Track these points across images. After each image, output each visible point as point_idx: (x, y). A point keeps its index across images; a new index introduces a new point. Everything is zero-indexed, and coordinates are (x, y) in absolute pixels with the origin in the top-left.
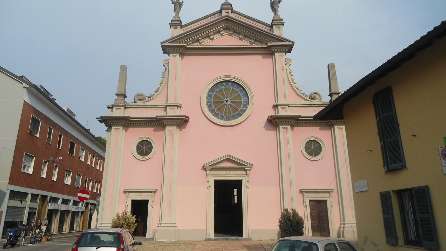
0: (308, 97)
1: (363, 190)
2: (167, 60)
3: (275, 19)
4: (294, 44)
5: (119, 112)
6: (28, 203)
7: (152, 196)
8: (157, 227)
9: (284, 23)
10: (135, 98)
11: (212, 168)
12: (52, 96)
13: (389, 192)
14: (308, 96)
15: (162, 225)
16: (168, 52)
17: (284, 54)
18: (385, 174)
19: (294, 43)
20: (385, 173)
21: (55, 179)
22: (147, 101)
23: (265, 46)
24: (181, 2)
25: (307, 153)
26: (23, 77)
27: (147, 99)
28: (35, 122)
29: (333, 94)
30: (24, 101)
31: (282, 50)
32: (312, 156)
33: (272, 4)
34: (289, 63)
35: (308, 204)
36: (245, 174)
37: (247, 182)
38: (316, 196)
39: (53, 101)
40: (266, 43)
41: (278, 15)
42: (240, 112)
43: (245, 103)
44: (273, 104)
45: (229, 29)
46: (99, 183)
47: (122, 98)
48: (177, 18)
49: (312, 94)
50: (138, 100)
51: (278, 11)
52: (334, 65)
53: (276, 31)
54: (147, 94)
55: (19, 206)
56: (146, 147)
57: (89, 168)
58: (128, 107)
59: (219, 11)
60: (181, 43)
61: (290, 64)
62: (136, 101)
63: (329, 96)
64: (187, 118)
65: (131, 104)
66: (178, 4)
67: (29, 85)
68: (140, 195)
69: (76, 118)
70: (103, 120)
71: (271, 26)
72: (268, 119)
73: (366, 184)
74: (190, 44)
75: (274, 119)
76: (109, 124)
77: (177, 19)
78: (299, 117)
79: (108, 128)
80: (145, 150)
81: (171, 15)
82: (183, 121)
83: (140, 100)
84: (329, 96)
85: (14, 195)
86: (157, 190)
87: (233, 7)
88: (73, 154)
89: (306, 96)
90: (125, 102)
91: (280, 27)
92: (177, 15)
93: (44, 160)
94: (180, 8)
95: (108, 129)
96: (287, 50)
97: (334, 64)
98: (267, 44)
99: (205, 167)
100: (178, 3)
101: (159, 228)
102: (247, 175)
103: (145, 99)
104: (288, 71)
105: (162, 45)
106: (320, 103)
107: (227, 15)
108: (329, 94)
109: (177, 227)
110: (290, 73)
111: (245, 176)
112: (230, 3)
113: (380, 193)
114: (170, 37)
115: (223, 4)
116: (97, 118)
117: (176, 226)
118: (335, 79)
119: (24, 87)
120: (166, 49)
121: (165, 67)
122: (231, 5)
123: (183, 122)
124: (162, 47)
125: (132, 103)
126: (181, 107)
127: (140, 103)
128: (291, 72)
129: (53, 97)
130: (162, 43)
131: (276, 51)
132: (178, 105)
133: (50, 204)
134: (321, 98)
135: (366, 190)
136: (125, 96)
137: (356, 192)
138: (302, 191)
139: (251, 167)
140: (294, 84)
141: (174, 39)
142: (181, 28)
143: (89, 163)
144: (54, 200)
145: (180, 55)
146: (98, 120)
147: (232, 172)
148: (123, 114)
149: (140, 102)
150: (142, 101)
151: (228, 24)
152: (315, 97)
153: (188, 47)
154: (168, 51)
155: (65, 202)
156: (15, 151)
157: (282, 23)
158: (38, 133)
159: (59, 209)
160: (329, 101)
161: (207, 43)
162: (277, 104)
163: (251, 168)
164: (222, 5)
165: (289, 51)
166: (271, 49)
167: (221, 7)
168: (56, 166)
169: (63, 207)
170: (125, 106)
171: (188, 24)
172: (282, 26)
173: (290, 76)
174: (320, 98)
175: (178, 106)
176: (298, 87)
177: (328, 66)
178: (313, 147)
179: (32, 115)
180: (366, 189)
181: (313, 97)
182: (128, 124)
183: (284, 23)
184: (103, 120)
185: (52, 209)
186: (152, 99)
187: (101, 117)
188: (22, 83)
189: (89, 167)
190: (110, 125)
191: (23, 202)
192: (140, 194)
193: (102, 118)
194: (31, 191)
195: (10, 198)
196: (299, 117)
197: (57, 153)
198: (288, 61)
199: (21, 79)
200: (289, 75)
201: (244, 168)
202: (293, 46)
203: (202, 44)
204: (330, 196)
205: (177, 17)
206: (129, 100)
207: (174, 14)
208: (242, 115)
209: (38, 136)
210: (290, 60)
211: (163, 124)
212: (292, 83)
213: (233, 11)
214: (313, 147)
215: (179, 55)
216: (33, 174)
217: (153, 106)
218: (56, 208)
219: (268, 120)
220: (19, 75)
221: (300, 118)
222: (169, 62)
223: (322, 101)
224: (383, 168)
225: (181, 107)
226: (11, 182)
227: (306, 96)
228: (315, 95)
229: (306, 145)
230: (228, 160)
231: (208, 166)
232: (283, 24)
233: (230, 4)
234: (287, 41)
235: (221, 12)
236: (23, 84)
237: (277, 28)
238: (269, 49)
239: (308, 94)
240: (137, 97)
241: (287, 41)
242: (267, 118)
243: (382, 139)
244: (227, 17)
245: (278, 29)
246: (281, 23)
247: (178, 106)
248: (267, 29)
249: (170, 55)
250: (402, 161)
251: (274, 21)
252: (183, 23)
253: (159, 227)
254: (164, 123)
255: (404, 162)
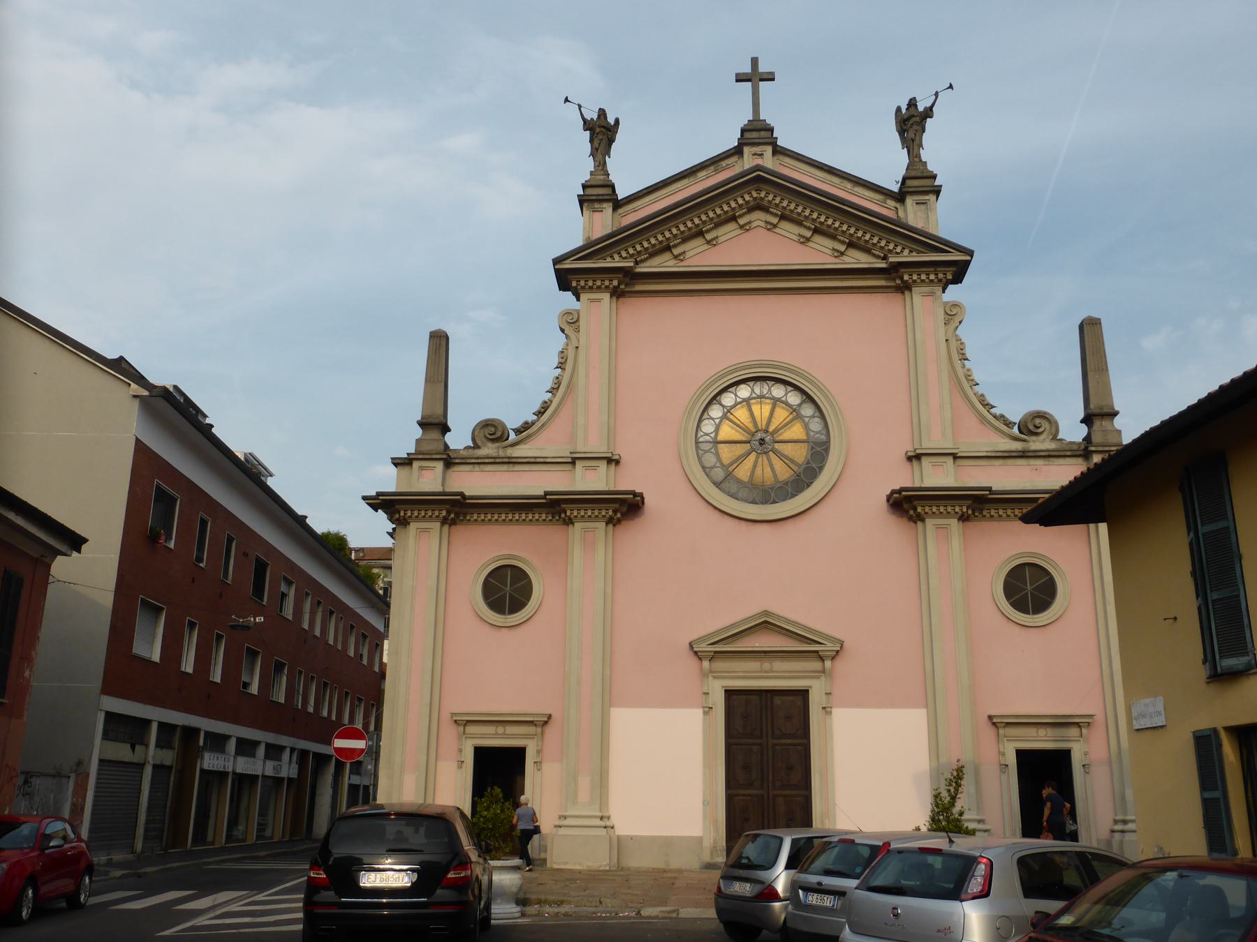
0: (1017, 425)
1: (1140, 725)
2: (571, 313)
3: (913, 174)
4: (972, 257)
5: (429, 480)
6: (152, 753)
7: (536, 735)
8: (555, 827)
9: (941, 186)
10: (476, 433)
11: (716, 652)
12: (206, 416)
13: (1215, 730)
14: (1015, 424)
15: (569, 822)
16: (576, 287)
17: (941, 289)
18: (1208, 683)
19: (971, 253)
20: (1208, 680)
21: (218, 679)
22: (514, 445)
23: (883, 265)
24: (612, 123)
25: (1011, 604)
26: (123, 362)
27: (512, 436)
28: (165, 500)
29: (1093, 417)
30: (137, 439)
31: (933, 278)
32: (1028, 613)
33: (902, 124)
34: (957, 320)
35: (1012, 759)
36: (821, 669)
37: (826, 694)
38: (1038, 736)
39: (206, 431)
40: (882, 255)
41: (921, 161)
42: (802, 476)
43: (818, 449)
44: (904, 454)
45: (765, 209)
46: (336, 687)
47: (435, 434)
48: (602, 177)
49: (1029, 420)
50: (484, 440)
51: (921, 145)
52: (1100, 324)
53: (912, 214)
54: (512, 422)
55: (127, 759)
56: (512, 588)
57: (305, 642)
58: (457, 461)
59: (733, 151)
60: (616, 260)
61: (960, 322)
62: (479, 443)
63: (1082, 422)
64: (638, 496)
65: (465, 453)
66: (604, 130)
67: (148, 390)
68: (500, 733)
69: (270, 482)
70: (380, 502)
71: (900, 197)
72: (889, 498)
73: (1160, 707)
74: (642, 261)
75: (909, 499)
76: (402, 513)
77: (600, 180)
78: (988, 493)
79: (394, 526)
80: (510, 594)
81: (584, 168)
82: (627, 505)
83: (493, 440)
84: (1082, 422)
85: (118, 726)
86: (550, 716)
87: (777, 138)
88: (262, 599)
89: (1010, 425)
90: (446, 447)
91: (929, 200)
92: (601, 166)
93: (188, 618)
94: (611, 141)
95: (397, 530)
96: (951, 278)
97: (1100, 319)
98: (885, 258)
99: (695, 649)
100: (603, 127)
101: (562, 831)
102: (824, 673)
103: (505, 438)
104: (954, 344)
105: (556, 267)
106: (1052, 446)
107: (758, 166)
108: (1081, 415)
109: (613, 828)
110: (957, 350)
111: (818, 677)
112: (768, 122)
113: (1194, 732)
114: (578, 242)
115: (746, 127)
116: (364, 498)
117: (612, 825)
118: (1103, 370)
119: (135, 396)
120: (565, 279)
121: (567, 337)
122: (772, 130)
123: (625, 509)
124: (557, 272)
125: (465, 448)
126: (617, 462)
127: (489, 450)
128: (962, 347)
129: (208, 421)
130: (556, 261)
131: (915, 281)
132: (610, 455)
133: (207, 755)
134: (1057, 431)
135: (1161, 724)
136: (445, 429)
137: (1138, 730)
138: (995, 720)
139: (839, 649)
140: (971, 387)
141: (592, 249)
142: (615, 209)
143: (306, 626)
144: (217, 741)
145: (611, 296)
146: (368, 504)
147: (779, 665)
148: (443, 485)
149: (490, 445)
150: (497, 444)
151: (763, 194)
152: (1039, 427)
153: (639, 270)
154: (574, 284)
155: (246, 747)
156: (115, 595)
157: (936, 189)
158: (171, 539)
159: (259, 773)
160: (1083, 440)
161: (698, 256)
162: (918, 451)
163: (837, 652)
164: (743, 131)
165: (958, 279)
166: (899, 274)
167: (739, 139)
168: (219, 637)
169: (244, 765)
170: (449, 458)
171: (637, 195)
172: (932, 197)
173: (957, 359)
174: (1054, 430)
175: (610, 461)
176: (982, 395)
177: (1081, 327)
178: (1028, 585)
179: (156, 480)
180: (1160, 721)
181: (1031, 428)
182: (457, 515)
183: (941, 186)
184: (380, 502)
185: (211, 769)
186: (529, 437)
187: (379, 494)
188: (126, 382)
189: (305, 636)
190: (405, 519)
191: (138, 748)
192: (500, 730)
193: (380, 498)
194: (156, 714)
195: (106, 736)
196: (988, 493)
197: (221, 595)
198: (953, 314)
199: (121, 367)
200: (956, 357)
201: (817, 652)
202: (966, 264)
203: (682, 260)
204: (1081, 736)
205: (602, 172)
206: (458, 439)
207: (590, 164)
208: (808, 486)
209: (172, 545)
210: (959, 306)
211: (563, 516)
212: (963, 383)
213: (778, 149)
214: (1028, 585)
215: (608, 295)
216: (160, 661)
217: (533, 460)
218: (222, 767)
219: (891, 501)
220: (111, 355)
221: (990, 494)
222: (577, 321)
223: (1060, 440)
224: (1202, 666)
225: (617, 462)
226: (110, 686)
227: (1009, 424)
228: (1037, 421)
229: (1008, 578)
230: (766, 624)
231: (704, 645)
232: (937, 191)
233: (768, 127)
234: (952, 250)
235: (738, 151)
236: (132, 386)
237: (917, 203)
238: (893, 275)
239: (1016, 417)
240: (482, 431)
241: (952, 250)
242: (887, 496)
243: (1201, 591)
244: (758, 173)
245: (923, 207)
246: (931, 189)
247: (610, 461)
248: (887, 209)
249: (583, 296)
250: (1247, 652)
251: (909, 183)
252: (622, 193)
253: (560, 827)
254: (568, 513)
255: (1251, 656)
